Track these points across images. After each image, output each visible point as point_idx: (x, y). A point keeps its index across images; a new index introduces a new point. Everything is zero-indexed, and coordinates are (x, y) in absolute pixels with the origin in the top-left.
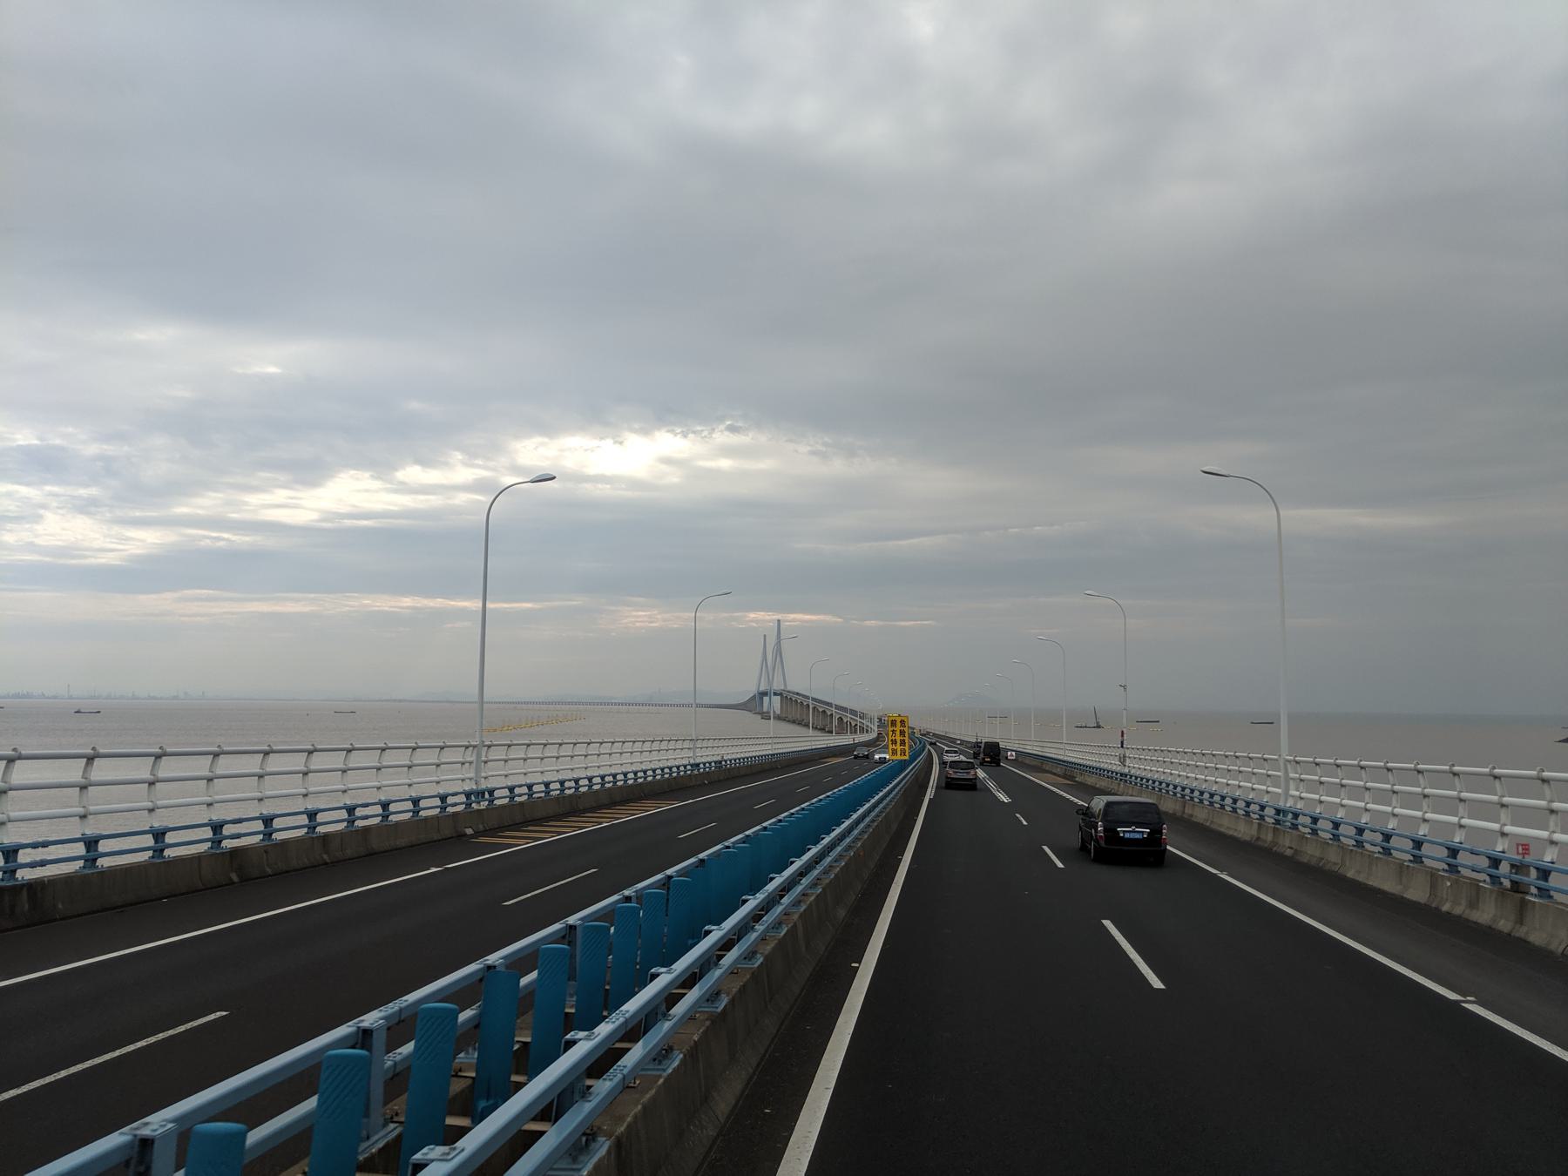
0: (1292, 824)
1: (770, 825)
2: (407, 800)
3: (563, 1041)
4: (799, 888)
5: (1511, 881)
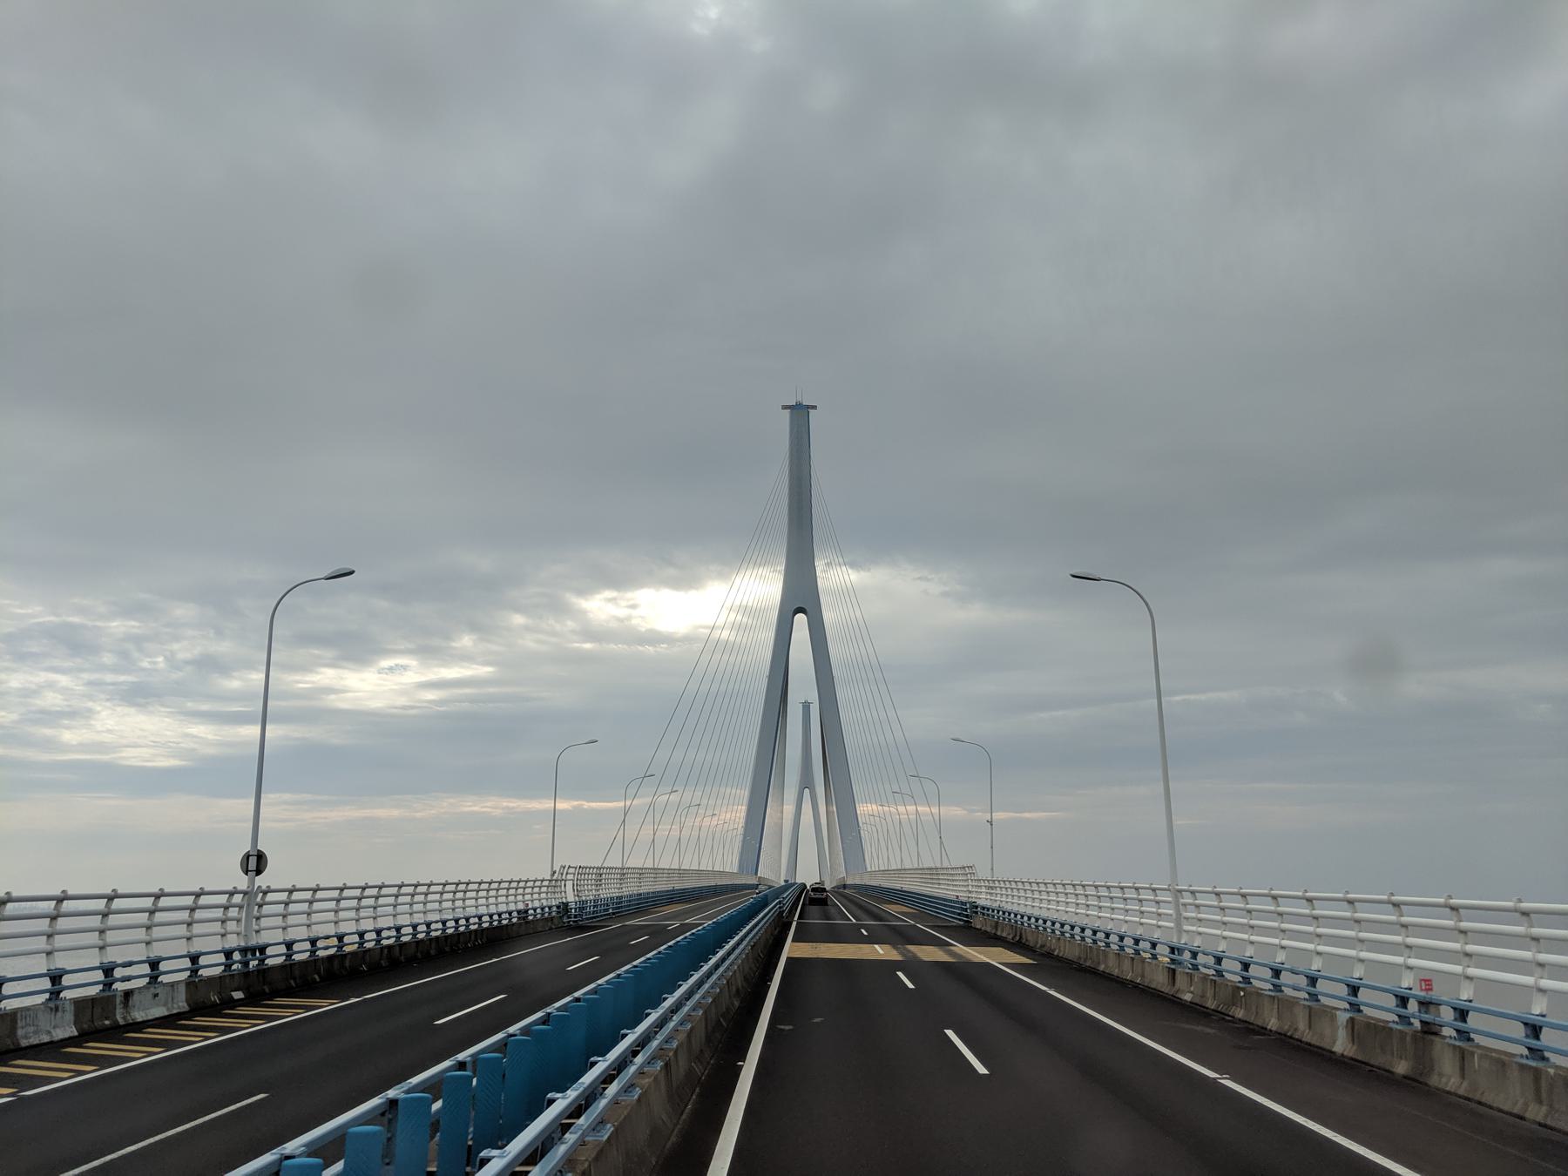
0: (1171, 959)
1: (640, 963)
2: (408, 926)
3: (478, 1159)
4: (671, 1025)
5: (1421, 1021)
